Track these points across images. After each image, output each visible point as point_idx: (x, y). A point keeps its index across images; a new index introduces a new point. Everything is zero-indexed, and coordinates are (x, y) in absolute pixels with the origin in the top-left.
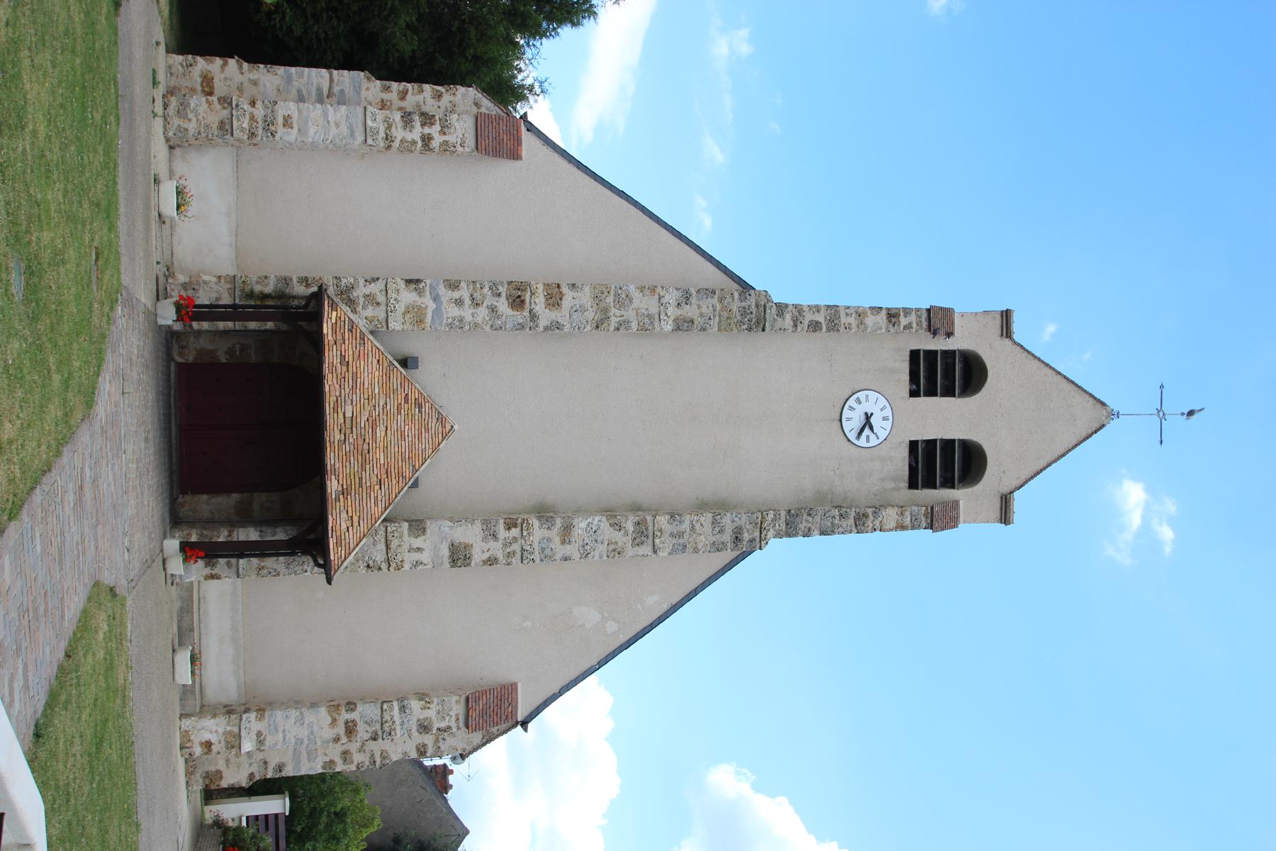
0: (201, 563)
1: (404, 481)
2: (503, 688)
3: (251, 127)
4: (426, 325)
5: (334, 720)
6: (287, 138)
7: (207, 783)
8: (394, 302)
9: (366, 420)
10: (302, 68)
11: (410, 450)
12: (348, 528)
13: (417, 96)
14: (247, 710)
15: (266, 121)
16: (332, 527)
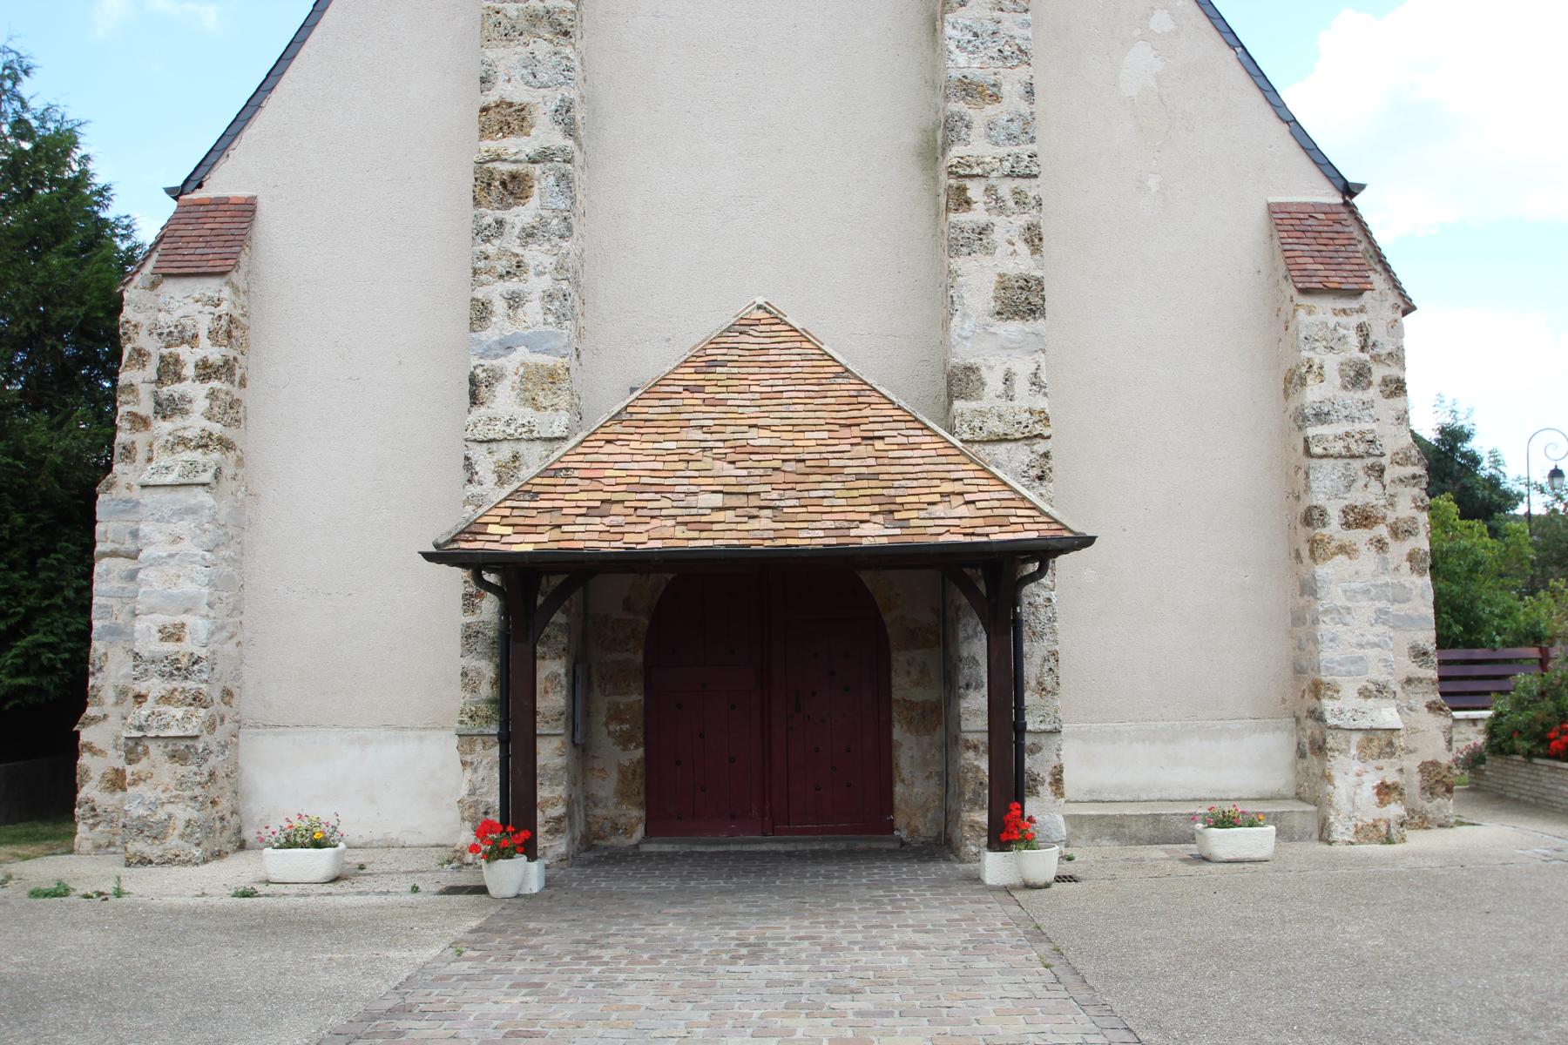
0: (1031, 806)
1: (868, 393)
2: (1280, 228)
3: (182, 702)
4: (559, 365)
5: (1342, 549)
6: (203, 635)
7: (1444, 789)
8: (513, 427)
9: (732, 466)
10: (94, 607)
11: (802, 382)
12: (967, 503)
13: (141, 396)
14: (1317, 716)
15: (172, 674)
16: (965, 534)
